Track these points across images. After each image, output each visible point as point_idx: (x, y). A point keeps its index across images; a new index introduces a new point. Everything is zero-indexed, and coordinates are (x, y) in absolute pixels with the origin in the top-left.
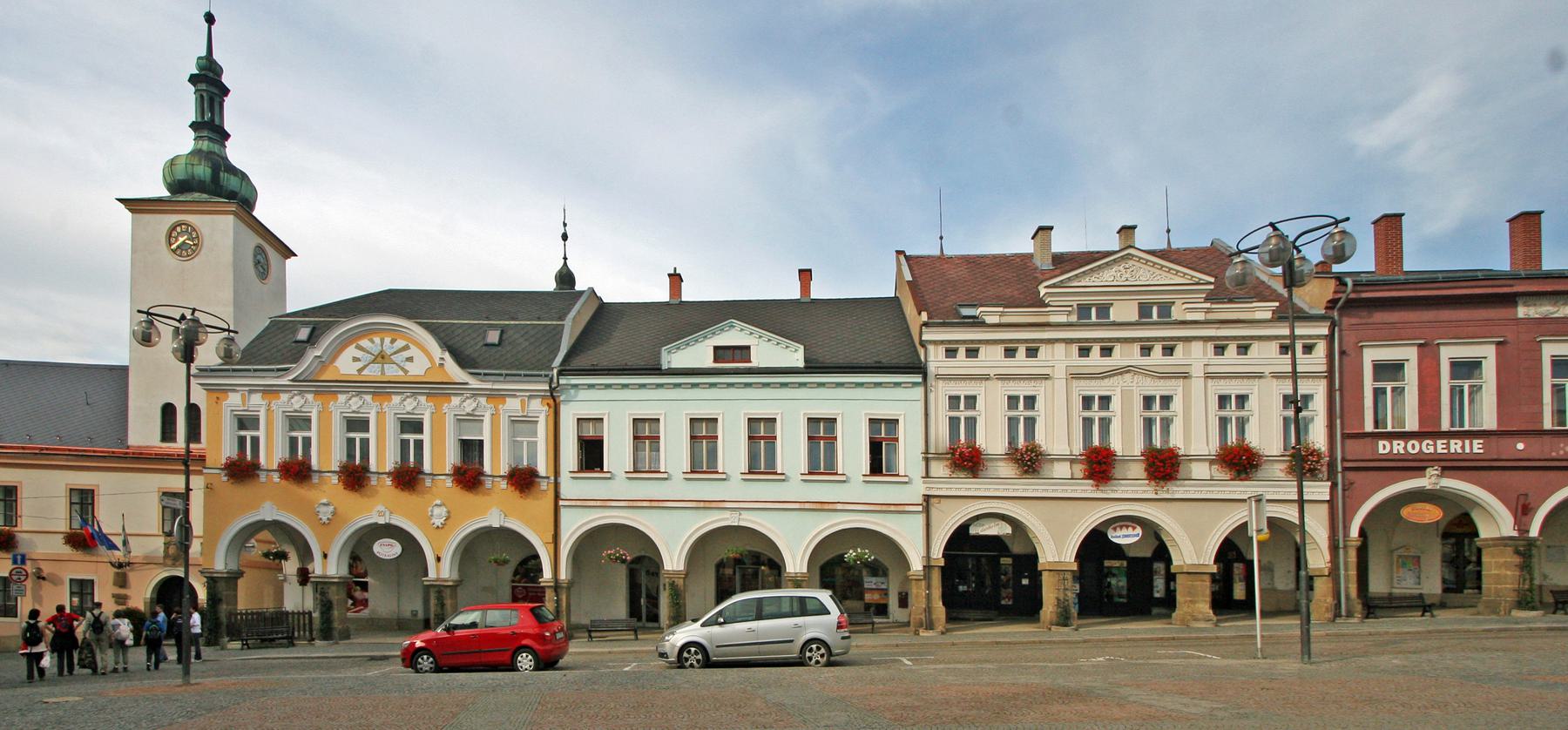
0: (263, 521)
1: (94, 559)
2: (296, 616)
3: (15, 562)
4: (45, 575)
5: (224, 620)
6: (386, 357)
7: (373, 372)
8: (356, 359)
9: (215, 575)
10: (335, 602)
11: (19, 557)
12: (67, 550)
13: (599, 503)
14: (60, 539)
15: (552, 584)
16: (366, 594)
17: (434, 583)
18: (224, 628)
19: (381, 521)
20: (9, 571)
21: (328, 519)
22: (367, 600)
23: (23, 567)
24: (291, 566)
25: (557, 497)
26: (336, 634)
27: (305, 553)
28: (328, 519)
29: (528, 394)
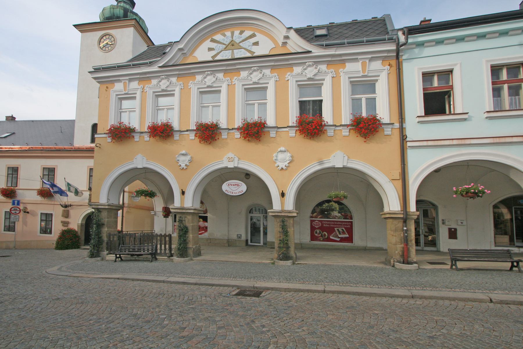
0: (136, 169)
1: (53, 203)
2: (159, 238)
3: (14, 204)
4: (28, 211)
5: (105, 239)
6: (235, 44)
7: (227, 55)
8: (210, 49)
9: (100, 207)
10: (190, 228)
11: (16, 202)
12: (39, 198)
13: (455, 142)
14: (35, 192)
15: (402, 216)
16: (206, 224)
17: (279, 214)
18: (105, 245)
19: (231, 165)
20: (10, 209)
21: (186, 165)
22: (206, 228)
23: (18, 206)
24: (158, 204)
25: (403, 138)
26: (190, 252)
27: (169, 196)
28: (186, 165)
29: (370, 56)
